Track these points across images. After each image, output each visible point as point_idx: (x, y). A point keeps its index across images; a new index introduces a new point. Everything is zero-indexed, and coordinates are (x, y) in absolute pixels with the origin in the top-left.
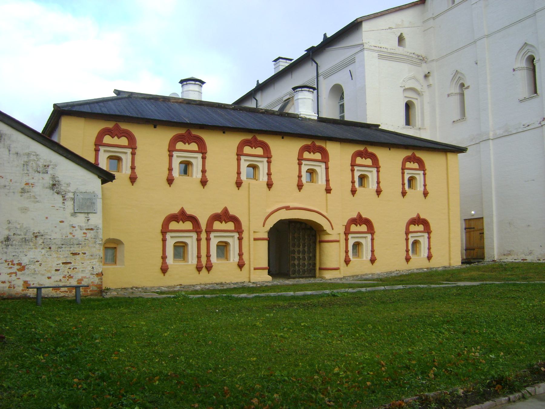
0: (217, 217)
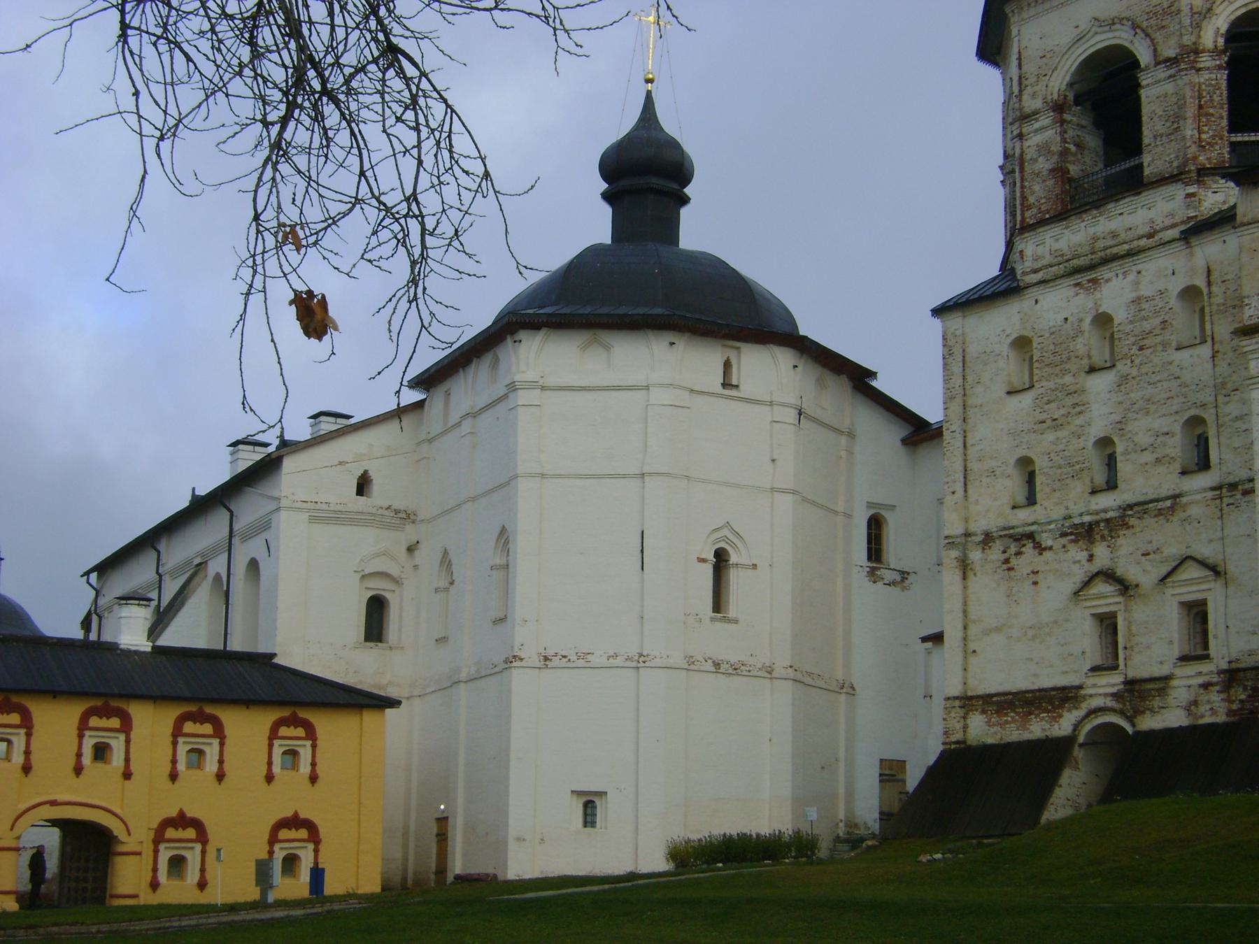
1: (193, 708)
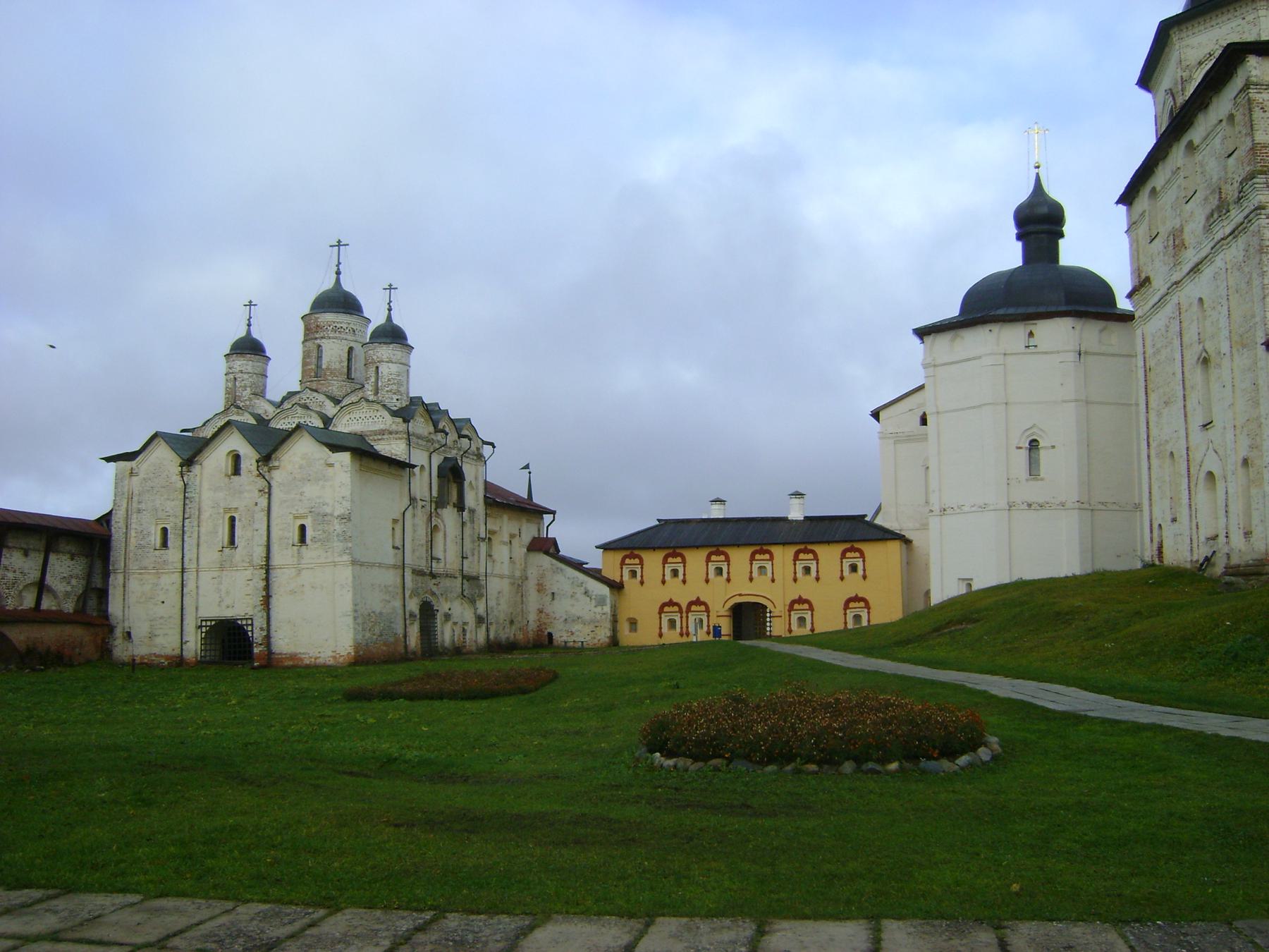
0: (691, 604)
1: (802, 547)
